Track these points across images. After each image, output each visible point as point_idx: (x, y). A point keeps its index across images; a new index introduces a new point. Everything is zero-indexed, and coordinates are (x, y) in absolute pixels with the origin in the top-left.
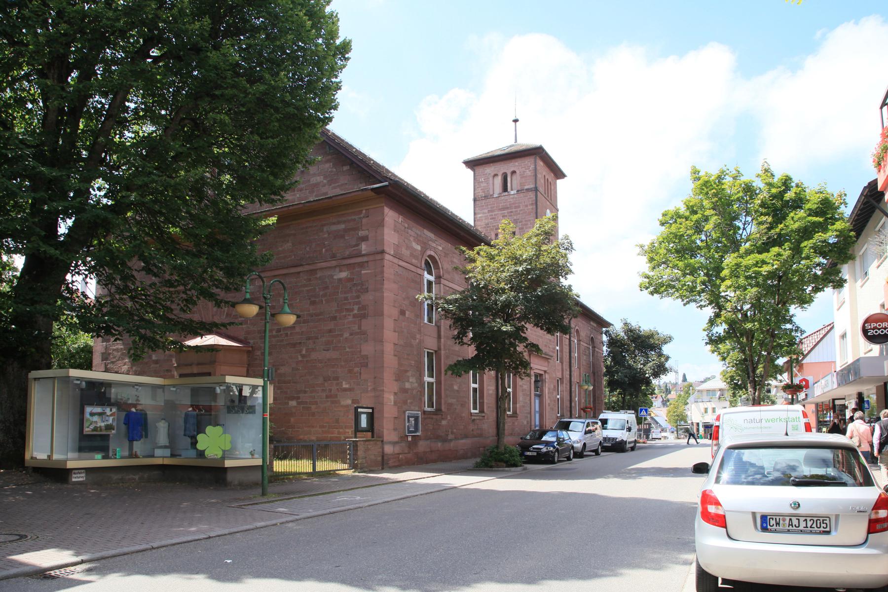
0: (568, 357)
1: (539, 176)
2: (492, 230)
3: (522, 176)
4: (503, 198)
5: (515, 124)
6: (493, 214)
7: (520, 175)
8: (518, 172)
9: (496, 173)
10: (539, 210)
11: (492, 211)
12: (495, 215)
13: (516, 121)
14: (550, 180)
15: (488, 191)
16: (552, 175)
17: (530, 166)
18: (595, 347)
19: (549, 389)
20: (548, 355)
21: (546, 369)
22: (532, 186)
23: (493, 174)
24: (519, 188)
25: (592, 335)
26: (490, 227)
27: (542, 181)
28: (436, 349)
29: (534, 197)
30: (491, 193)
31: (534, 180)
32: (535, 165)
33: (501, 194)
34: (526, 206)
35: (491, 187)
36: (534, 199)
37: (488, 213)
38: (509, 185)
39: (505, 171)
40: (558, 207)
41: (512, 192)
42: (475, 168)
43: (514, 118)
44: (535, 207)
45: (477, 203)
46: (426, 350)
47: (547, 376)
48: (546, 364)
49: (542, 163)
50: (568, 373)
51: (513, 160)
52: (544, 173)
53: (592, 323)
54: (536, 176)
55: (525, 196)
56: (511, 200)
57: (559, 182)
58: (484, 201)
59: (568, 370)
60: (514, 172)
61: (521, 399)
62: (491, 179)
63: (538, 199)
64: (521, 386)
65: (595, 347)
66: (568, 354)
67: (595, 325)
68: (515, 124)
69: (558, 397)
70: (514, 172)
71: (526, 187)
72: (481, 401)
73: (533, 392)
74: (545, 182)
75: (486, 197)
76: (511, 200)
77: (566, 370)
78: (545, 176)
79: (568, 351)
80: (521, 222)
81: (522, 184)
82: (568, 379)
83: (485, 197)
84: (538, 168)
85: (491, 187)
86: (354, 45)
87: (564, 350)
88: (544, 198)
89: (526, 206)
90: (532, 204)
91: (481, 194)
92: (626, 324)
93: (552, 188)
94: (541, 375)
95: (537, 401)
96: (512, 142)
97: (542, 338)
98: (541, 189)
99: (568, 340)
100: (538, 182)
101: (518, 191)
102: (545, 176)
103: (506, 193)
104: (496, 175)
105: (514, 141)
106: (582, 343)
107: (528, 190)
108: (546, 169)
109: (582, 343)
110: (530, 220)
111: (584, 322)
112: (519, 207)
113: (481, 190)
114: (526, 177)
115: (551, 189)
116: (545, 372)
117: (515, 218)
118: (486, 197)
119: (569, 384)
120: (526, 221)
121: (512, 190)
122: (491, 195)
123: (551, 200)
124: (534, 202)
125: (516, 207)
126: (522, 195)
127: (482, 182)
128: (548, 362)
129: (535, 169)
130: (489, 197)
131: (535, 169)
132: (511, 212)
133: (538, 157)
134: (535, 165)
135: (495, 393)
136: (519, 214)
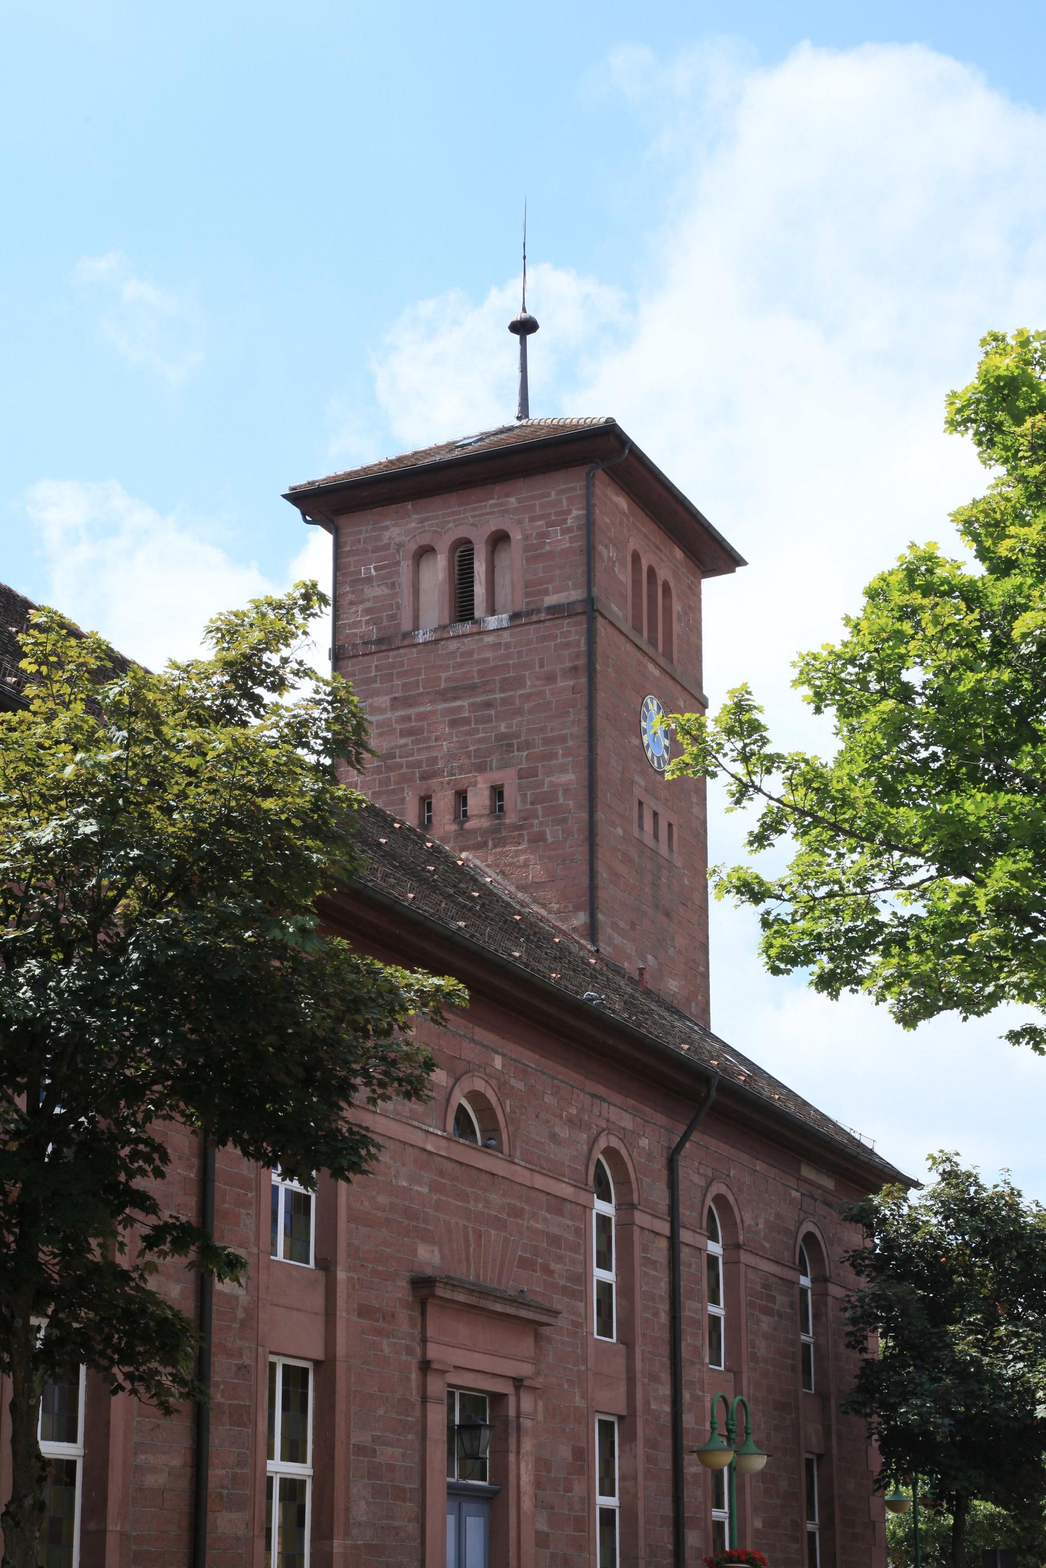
0: (664, 1318)
1: (606, 552)
2: (405, 779)
3: (534, 554)
4: (453, 646)
5: (523, 343)
6: (412, 711)
7: (526, 549)
8: (516, 536)
9: (425, 540)
10: (601, 696)
11: (407, 702)
12: (421, 717)
13: (524, 327)
14: (663, 574)
15: (393, 617)
16: (679, 554)
17: (569, 512)
18: (826, 1280)
19: (542, 1464)
20: (527, 1305)
21: (525, 1369)
22: (576, 595)
23: (413, 547)
24: (521, 606)
25: (808, 1227)
26: (400, 766)
27: (625, 576)
28: (319, 1354)
29: (583, 641)
30: (407, 626)
31: (581, 570)
32: (589, 508)
33: (443, 628)
34: (551, 678)
35: (405, 598)
36: (583, 647)
37: (393, 708)
38: (479, 590)
39: (462, 532)
40: (706, 691)
41: (492, 622)
42: (342, 521)
43: (517, 316)
44: (583, 680)
45: (349, 666)
46: (280, 1362)
47: (527, 1402)
48: (527, 1345)
49: (622, 502)
50: (665, 1390)
51: (497, 488)
52: (633, 544)
53: (806, 1172)
54: (590, 552)
55: (545, 638)
56: (489, 655)
57: (710, 586)
58: (374, 661)
59: (665, 1376)
60: (499, 539)
61: (361, 1511)
62: (406, 567)
63: (600, 649)
64: (360, 1450)
65: (826, 1280)
66: (664, 1308)
67: (829, 1184)
68: (523, 343)
69: (720, 1515)
70: (499, 539)
71: (550, 600)
72: (92, 1526)
73: (438, 1480)
74: (636, 582)
75: (385, 643)
76: (489, 655)
77: (654, 1378)
78: (636, 558)
79: (663, 1288)
80: (528, 745)
81: (532, 588)
82: (666, 1421)
83: (379, 641)
84: (603, 519)
85: (405, 598)
86: (954, 509)
87: (640, 1286)
88: (629, 647)
89: (551, 678)
90: (575, 668)
91: (364, 629)
92: (950, 1176)
93: (677, 607)
94: (498, 1399)
95: (475, 1527)
96: (508, 417)
97: (500, 1224)
98: (618, 610)
99: (663, 1244)
100: (600, 577)
101: (515, 616)
102: (636, 558)
103: (468, 627)
104: (425, 552)
105: (515, 410)
106: (745, 1257)
107: (557, 611)
108: (648, 527)
109: (745, 1257)
110: (563, 739)
111: (759, 1166)
112: (520, 682)
113: (367, 611)
114: (551, 555)
115: (668, 610)
116: (518, 1383)
117: (503, 728)
118: (385, 643)
119: (668, 1442)
120: (546, 741)
121: (492, 611)
122: (406, 635)
123: (668, 655)
124: (582, 662)
125: (506, 685)
126: (531, 632)
127: (369, 580)
128: (538, 1337)
129: (589, 525)
130: (398, 642)
131: (589, 525)
132: (488, 705)
133: (600, 474)
134: (589, 508)
135: (184, 1484)
136: (520, 712)
